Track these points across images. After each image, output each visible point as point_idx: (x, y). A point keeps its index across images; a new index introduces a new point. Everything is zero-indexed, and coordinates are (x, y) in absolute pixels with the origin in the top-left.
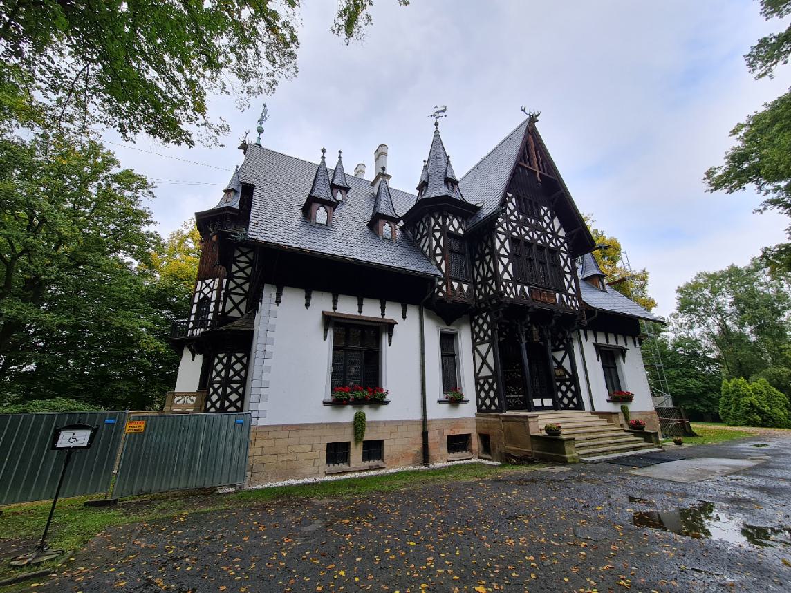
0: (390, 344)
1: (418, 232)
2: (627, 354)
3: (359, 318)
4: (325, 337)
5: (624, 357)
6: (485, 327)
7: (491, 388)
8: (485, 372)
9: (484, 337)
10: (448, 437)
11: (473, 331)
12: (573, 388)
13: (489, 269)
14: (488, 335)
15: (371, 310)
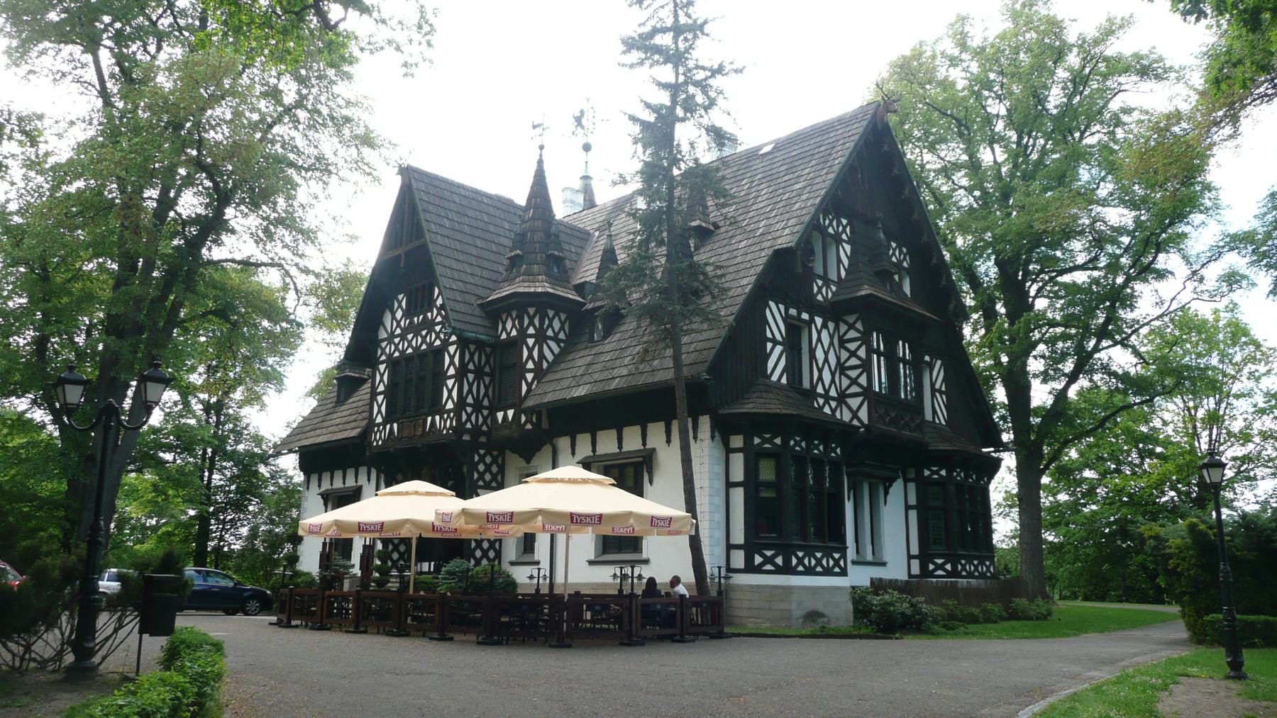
1: (504, 329)
7: (481, 476)
14: (944, 564)
15: (632, 441)
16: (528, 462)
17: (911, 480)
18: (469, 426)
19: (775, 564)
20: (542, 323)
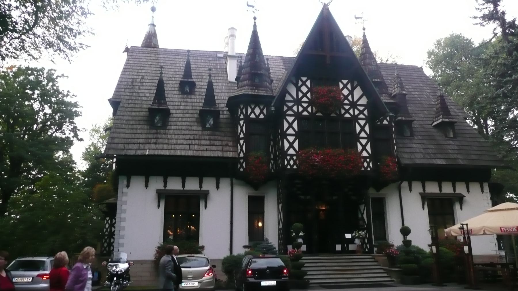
0: (206, 207)
4: (159, 206)
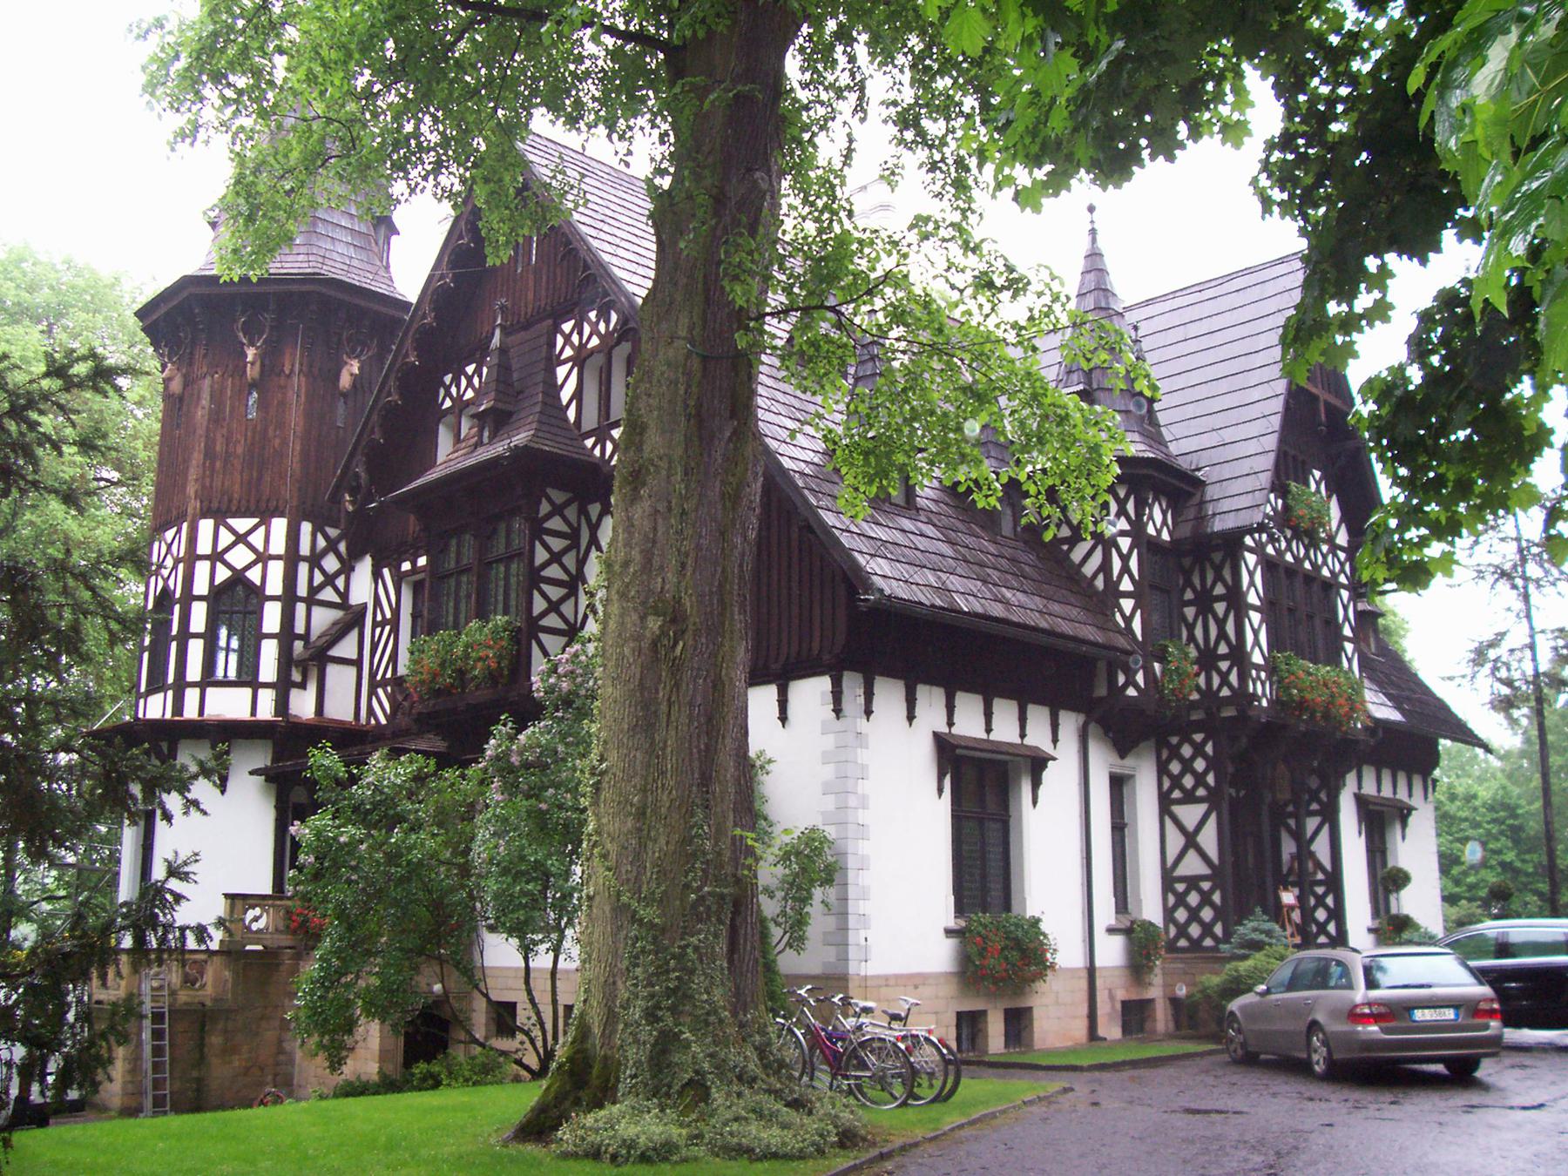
0: (1035, 803)
2: (1046, 775)
3: (985, 746)
4: (940, 791)
5: (1404, 825)
6: (1200, 765)
7: (1206, 899)
8: (1192, 865)
9: (1195, 788)
10: (1123, 1003)
11: (1162, 770)
12: (1330, 901)
13: (1222, 635)
16: (1122, 757)
17: (299, 637)
18: (1225, 692)
19: (1171, 790)
20: (1139, 514)
